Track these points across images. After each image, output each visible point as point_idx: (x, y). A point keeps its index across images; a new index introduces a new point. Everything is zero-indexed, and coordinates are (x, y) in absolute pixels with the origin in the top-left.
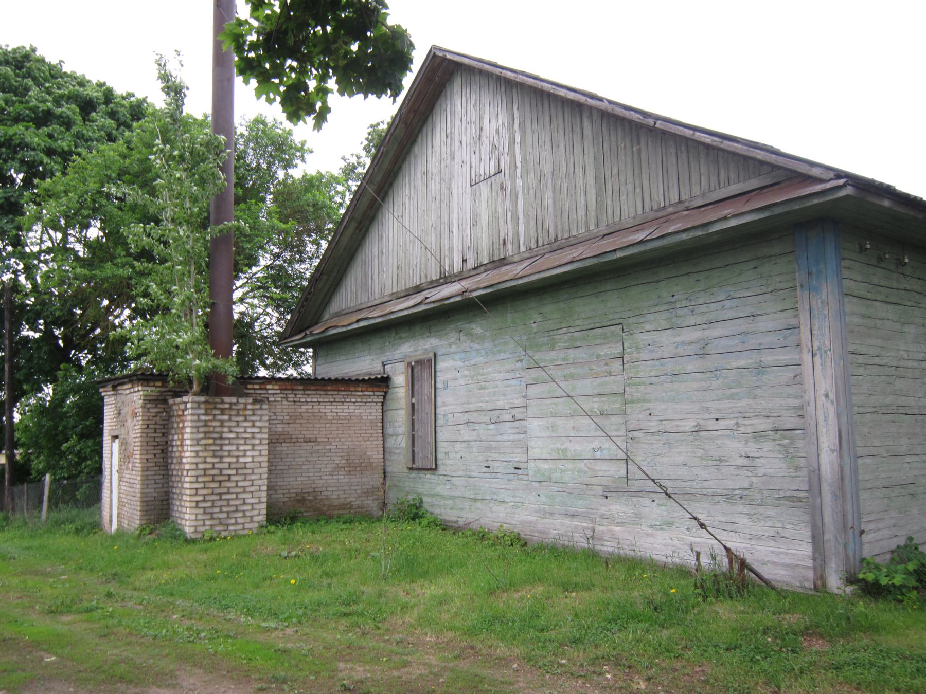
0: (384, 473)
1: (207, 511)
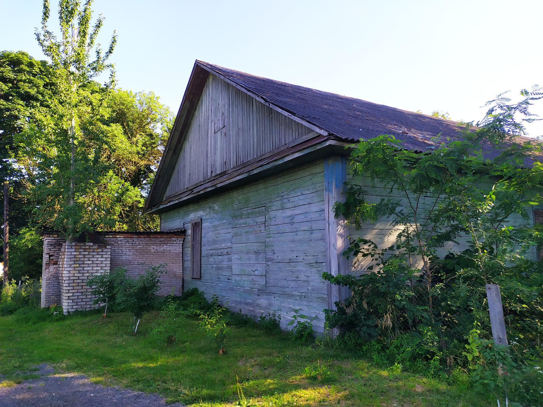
0: (183, 280)
1: (74, 301)
